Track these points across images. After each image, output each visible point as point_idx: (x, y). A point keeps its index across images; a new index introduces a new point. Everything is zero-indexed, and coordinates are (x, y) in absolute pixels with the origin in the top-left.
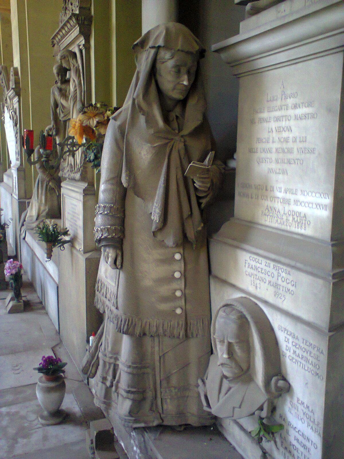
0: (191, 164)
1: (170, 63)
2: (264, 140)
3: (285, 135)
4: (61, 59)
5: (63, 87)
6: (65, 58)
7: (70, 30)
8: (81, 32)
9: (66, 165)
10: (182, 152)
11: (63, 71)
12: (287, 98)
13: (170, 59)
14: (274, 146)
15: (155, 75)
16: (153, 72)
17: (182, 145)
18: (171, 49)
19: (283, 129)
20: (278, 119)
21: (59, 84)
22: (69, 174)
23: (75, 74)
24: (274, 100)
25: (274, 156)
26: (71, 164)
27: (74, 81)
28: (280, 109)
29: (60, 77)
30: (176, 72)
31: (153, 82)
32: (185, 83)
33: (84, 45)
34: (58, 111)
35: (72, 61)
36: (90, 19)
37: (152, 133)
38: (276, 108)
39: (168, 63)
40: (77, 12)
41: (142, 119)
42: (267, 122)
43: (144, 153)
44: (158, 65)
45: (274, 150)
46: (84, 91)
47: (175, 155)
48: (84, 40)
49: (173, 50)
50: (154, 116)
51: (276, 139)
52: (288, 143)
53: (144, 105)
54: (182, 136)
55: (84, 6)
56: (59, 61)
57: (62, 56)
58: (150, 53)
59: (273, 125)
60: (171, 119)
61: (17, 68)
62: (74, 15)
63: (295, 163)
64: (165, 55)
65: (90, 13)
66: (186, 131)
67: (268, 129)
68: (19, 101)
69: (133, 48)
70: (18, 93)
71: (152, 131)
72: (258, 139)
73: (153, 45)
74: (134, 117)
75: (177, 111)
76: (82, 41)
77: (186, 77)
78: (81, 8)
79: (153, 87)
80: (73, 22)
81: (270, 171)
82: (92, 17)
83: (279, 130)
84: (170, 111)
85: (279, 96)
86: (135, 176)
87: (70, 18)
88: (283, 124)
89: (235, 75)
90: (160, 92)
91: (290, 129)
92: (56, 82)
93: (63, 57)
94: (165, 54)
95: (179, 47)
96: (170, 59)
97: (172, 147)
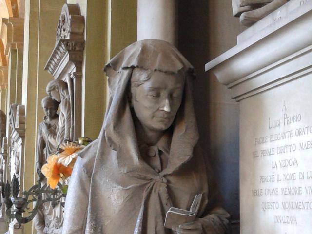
0: (169, 211)
1: (147, 86)
2: (268, 179)
3: (291, 170)
4: (50, 91)
5: (53, 122)
6: (54, 89)
7: (61, 58)
8: (71, 60)
9: (52, 218)
10: (165, 196)
11: (53, 106)
12: (290, 123)
13: (145, 81)
14: (280, 186)
15: (130, 102)
16: (127, 97)
17: (163, 189)
18: (147, 69)
19: (289, 162)
20: (282, 150)
21: (48, 120)
22: (53, 230)
23: (64, 107)
24: (276, 126)
25: (280, 199)
26: (57, 217)
27: (63, 115)
28: (284, 137)
29: (48, 111)
30: (154, 96)
31: (128, 109)
32: (166, 109)
33: (74, 73)
34: (45, 152)
35: (63, 93)
36: (82, 44)
37: (126, 172)
38: (279, 136)
39: (144, 85)
40: (68, 38)
41: (113, 154)
42: (270, 155)
43: (114, 197)
44: (134, 90)
45: (280, 192)
46: (73, 126)
47: (154, 199)
48: (75, 68)
49: (149, 70)
50: (128, 151)
51: (282, 177)
52: (295, 181)
53: (115, 138)
54: (165, 176)
55: (77, 30)
56: (48, 93)
57: (50, 88)
58: (122, 75)
59: (277, 158)
60: (152, 154)
61: (24, 106)
62: (62, 41)
63: (304, 207)
64: (140, 76)
65: (83, 38)
66: (169, 170)
67: (271, 163)
68: (23, 145)
69: (105, 70)
70: (22, 136)
71: (125, 170)
72: (262, 177)
73: (126, 66)
74: (103, 154)
75: (161, 144)
76: (73, 69)
77: (167, 102)
78: (72, 34)
79: (127, 116)
80: (63, 48)
81: (278, 219)
82: (85, 41)
83: (285, 164)
84: (152, 144)
85: (282, 121)
86: (102, 226)
87: (59, 45)
88: (288, 156)
89: (234, 98)
90: (136, 122)
91: (295, 163)
92: (45, 118)
93: (52, 88)
94: (140, 75)
95: (157, 66)
96: (145, 81)
97: (151, 189)
